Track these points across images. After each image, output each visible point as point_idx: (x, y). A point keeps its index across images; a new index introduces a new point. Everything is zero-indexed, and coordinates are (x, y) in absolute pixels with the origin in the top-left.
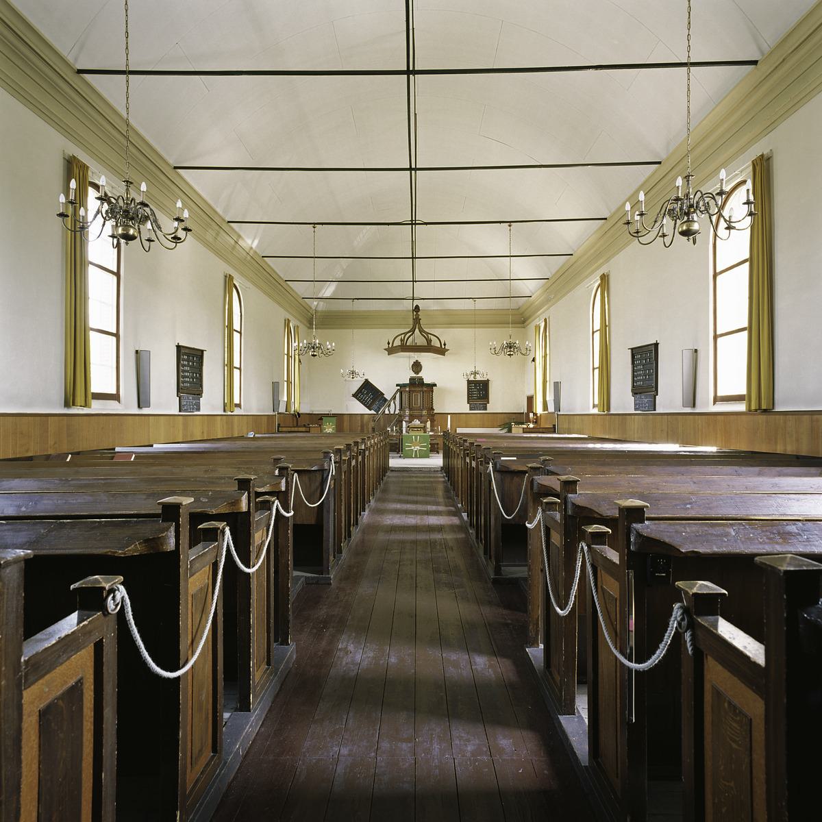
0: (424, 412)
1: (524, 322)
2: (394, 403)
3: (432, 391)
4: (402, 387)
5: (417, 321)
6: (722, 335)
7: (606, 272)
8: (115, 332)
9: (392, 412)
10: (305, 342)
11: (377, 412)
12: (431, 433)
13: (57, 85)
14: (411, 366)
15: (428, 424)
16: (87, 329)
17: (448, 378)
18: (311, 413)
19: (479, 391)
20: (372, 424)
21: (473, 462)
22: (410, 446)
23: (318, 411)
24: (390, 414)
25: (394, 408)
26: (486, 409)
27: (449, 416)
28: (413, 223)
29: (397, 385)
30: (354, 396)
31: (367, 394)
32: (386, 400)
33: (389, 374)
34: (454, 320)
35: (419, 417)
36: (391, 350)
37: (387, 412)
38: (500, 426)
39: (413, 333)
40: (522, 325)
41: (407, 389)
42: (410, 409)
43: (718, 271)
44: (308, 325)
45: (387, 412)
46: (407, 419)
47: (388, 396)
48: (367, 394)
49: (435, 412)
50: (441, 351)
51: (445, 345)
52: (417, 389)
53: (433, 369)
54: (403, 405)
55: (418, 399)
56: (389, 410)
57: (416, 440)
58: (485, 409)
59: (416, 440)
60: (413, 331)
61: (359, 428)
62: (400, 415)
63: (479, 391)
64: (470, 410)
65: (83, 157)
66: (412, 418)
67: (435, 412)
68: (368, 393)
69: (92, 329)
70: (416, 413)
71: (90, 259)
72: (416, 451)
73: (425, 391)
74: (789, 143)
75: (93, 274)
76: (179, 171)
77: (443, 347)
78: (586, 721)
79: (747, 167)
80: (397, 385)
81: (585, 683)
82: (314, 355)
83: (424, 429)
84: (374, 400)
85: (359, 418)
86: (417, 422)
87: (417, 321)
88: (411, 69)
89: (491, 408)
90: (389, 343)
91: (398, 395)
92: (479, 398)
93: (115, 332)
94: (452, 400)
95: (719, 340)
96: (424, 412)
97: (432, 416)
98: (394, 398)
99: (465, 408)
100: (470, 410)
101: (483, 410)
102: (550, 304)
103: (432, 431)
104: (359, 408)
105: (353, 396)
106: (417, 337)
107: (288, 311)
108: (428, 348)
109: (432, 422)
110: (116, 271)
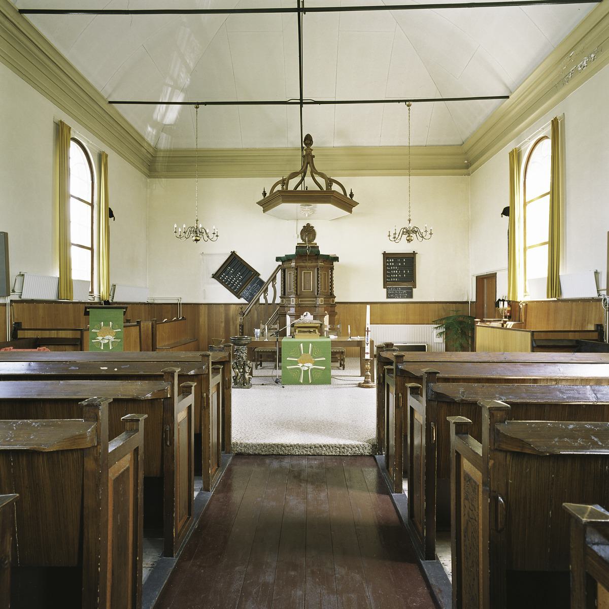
0: (320, 301)
1: (467, 167)
2: (274, 286)
3: (332, 269)
4: (285, 260)
5: (308, 159)
6: (530, 247)
7: (559, 115)
8: (90, 246)
9: (270, 301)
10: (184, 226)
11: (249, 301)
12: (333, 337)
13: (46, 65)
14: (299, 233)
15: (326, 319)
16: (68, 244)
17: (355, 247)
18: (150, 301)
19: (400, 270)
20: (239, 320)
21: (411, 401)
22: (296, 363)
23: (162, 299)
24: (267, 304)
25: (272, 295)
26: (411, 297)
27: (368, 307)
28: (301, 103)
29: (278, 259)
30: (215, 276)
31: (235, 273)
32: (261, 283)
33: (266, 242)
34: (367, 161)
35: (312, 309)
36: (267, 203)
37: (262, 301)
38: (434, 322)
39: (303, 179)
40: (464, 171)
41: (293, 264)
42: (298, 296)
43: (527, 201)
44: (147, 171)
45: (262, 301)
46: (292, 311)
47: (264, 277)
48: (235, 273)
49: (336, 300)
50: (346, 203)
51: (352, 195)
52: (308, 264)
53: (334, 233)
54: (287, 290)
55: (310, 279)
56: (265, 298)
57: (306, 351)
58: (410, 295)
59: (306, 351)
60: (304, 173)
61: (223, 325)
62: (282, 306)
63: (400, 270)
64: (388, 297)
65: (68, 121)
66: (300, 310)
67: (336, 300)
68: (235, 272)
69: (73, 244)
70: (307, 302)
71: (72, 193)
72: (306, 372)
73: (322, 267)
74: (575, 107)
75: (74, 204)
76: (27, 16)
77: (348, 196)
78: (450, 579)
79: (548, 125)
80: (278, 259)
81: (407, 477)
82: (197, 240)
83: (320, 328)
84: (244, 283)
85: (222, 309)
86: (308, 318)
87: (308, 159)
88: (299, 101)
89: (419, 295)
90: (264, 194)
91: (279, 275)
92: (402, 280)
93: (90, 246)
94: (359, 282)
95: (528, 252)
96: (320, 301)
97: (332, 307)
98: (273, 279)
99: (380, 294)
100: (388, 297)
101: (407, 297)
102: (569, 86)
103: (332, 330)
104: (221, 295)
105: (214, 276)
106: (307, 181)
107: (103, 140)
108: (325, 196)
109: (332, 315)
110: (91, 202)
